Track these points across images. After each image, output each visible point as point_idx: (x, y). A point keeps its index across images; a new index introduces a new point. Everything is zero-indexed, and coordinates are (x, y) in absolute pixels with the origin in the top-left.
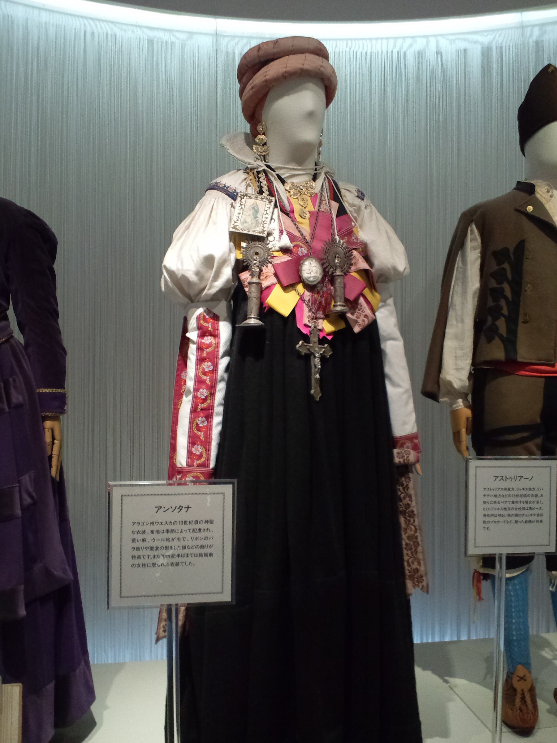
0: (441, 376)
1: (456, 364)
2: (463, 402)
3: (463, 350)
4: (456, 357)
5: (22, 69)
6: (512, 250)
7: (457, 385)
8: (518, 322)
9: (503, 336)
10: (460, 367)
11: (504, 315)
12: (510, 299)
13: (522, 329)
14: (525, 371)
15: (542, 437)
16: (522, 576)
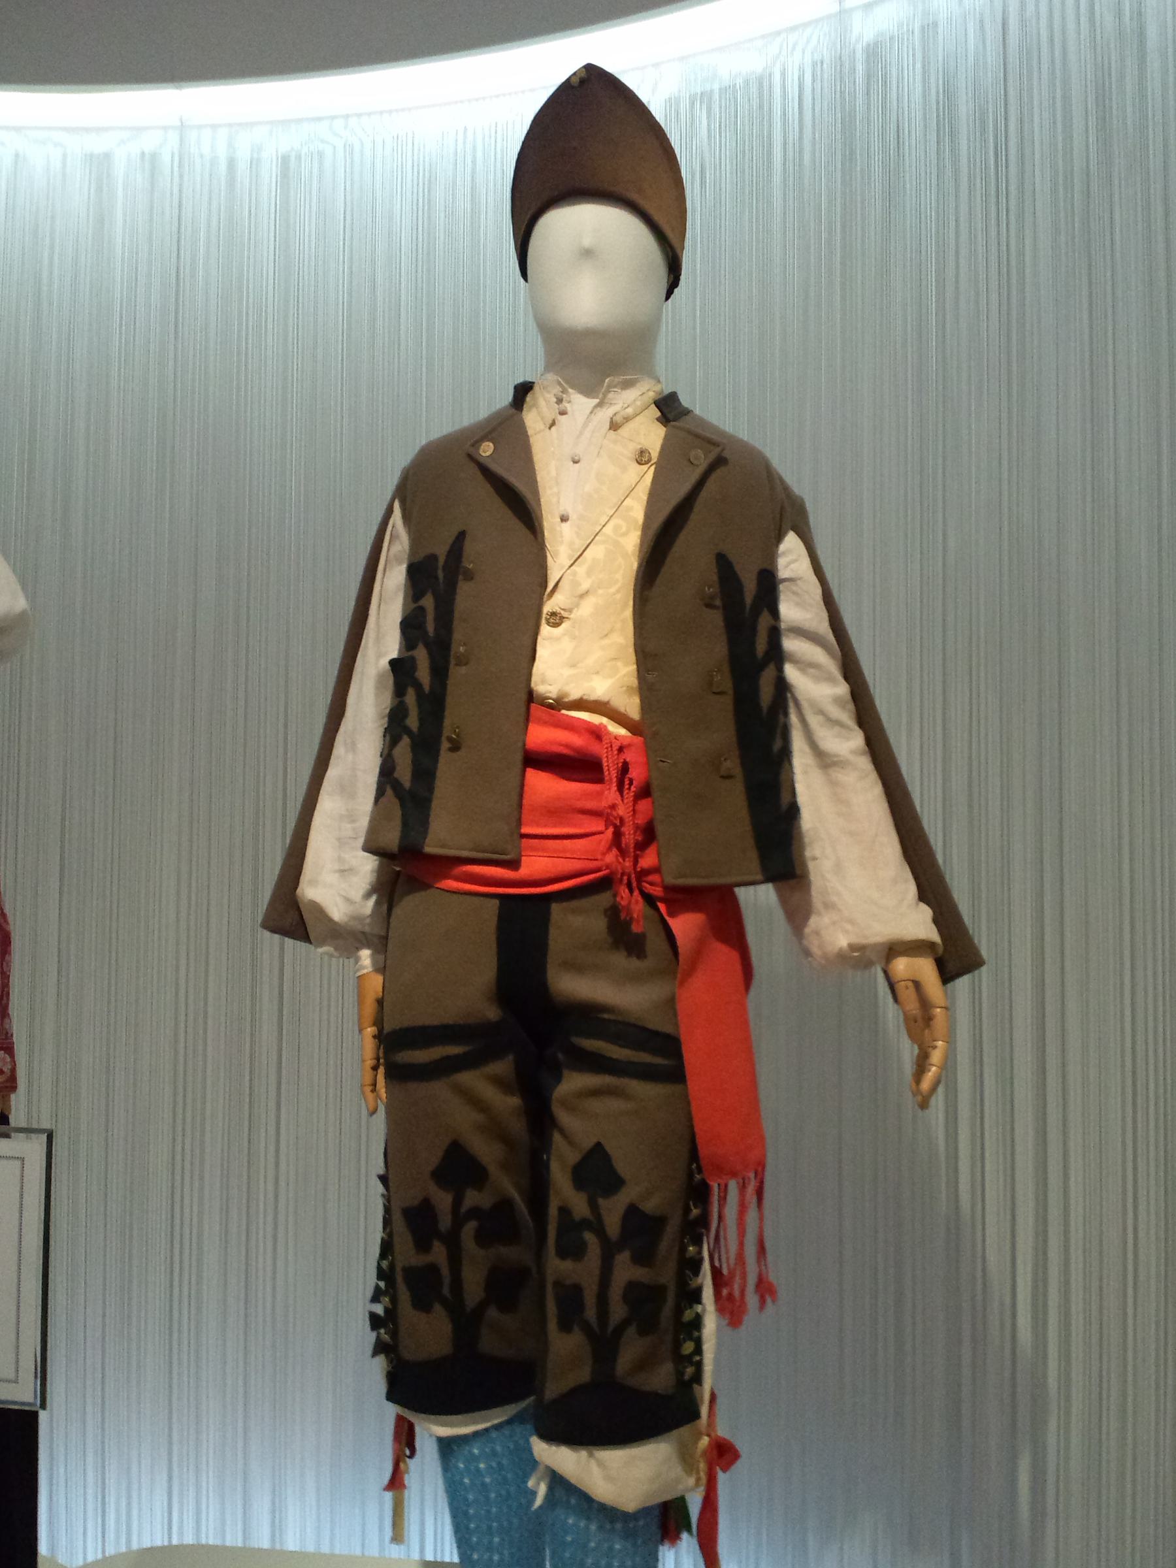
0: (299, 891)
1: (340, 860)
2: (372, 956)
3: (353, 821)
4: (339, 839)
5: (427, 159)
6: (441, 561)
7: (338, 912)
8: (438, 751)
9: (401, 785)
10: (346, 867)
11: (409, 732)
12: (427, 688)
13: (447, 766)
14: (458, 879)
15: (511, 1057)
16: (494, 1434)
